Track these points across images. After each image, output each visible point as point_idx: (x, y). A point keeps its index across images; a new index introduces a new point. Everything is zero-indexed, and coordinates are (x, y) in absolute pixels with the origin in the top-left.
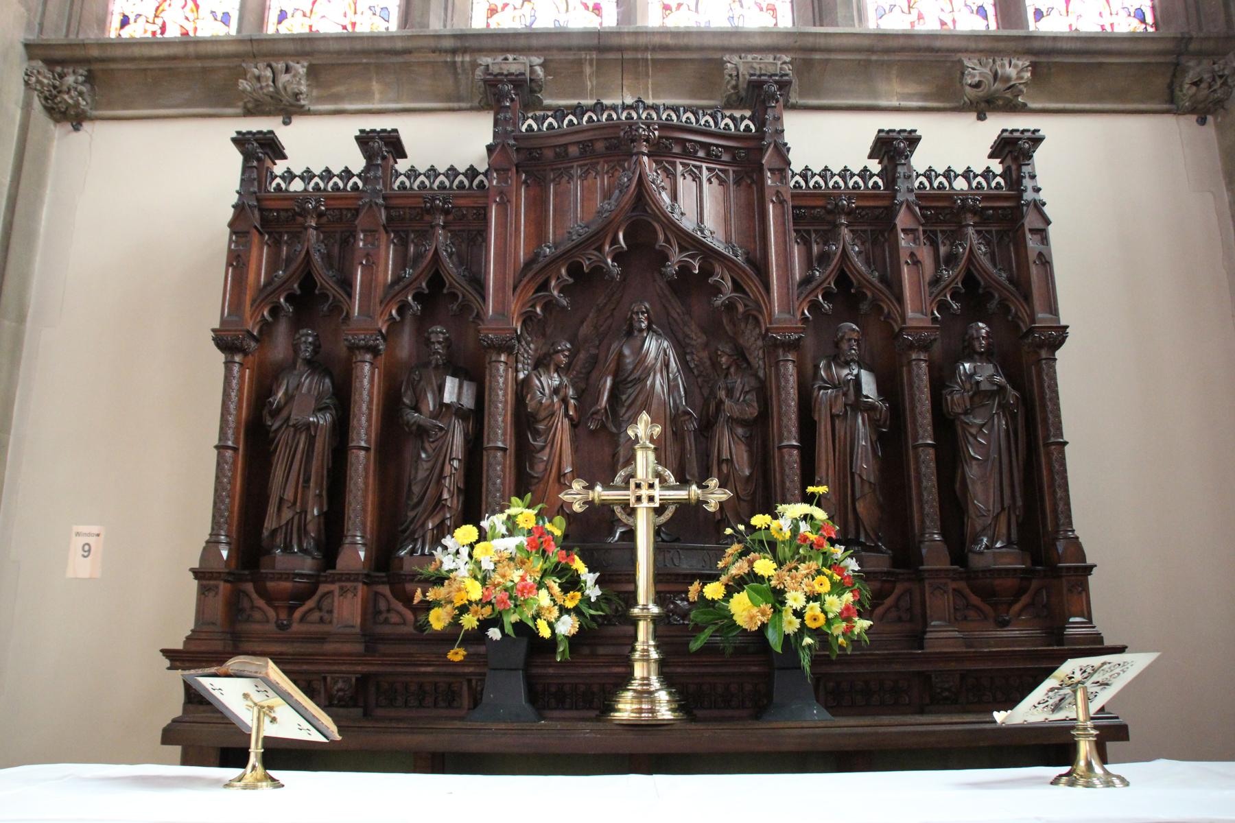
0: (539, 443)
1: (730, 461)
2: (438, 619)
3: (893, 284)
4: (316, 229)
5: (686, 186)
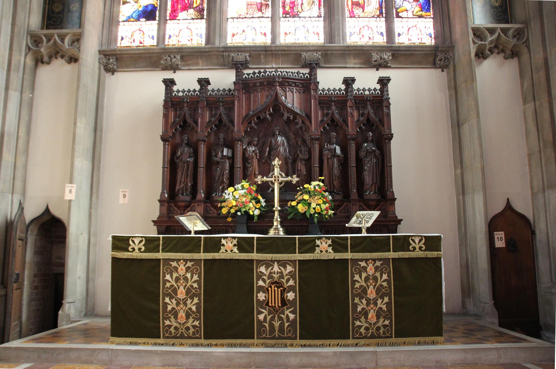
0: (249, 166)
1: (300, 170)
2: (224, 211)
3: (345, 121)
4: (187, 107)
5: (289, 94)
